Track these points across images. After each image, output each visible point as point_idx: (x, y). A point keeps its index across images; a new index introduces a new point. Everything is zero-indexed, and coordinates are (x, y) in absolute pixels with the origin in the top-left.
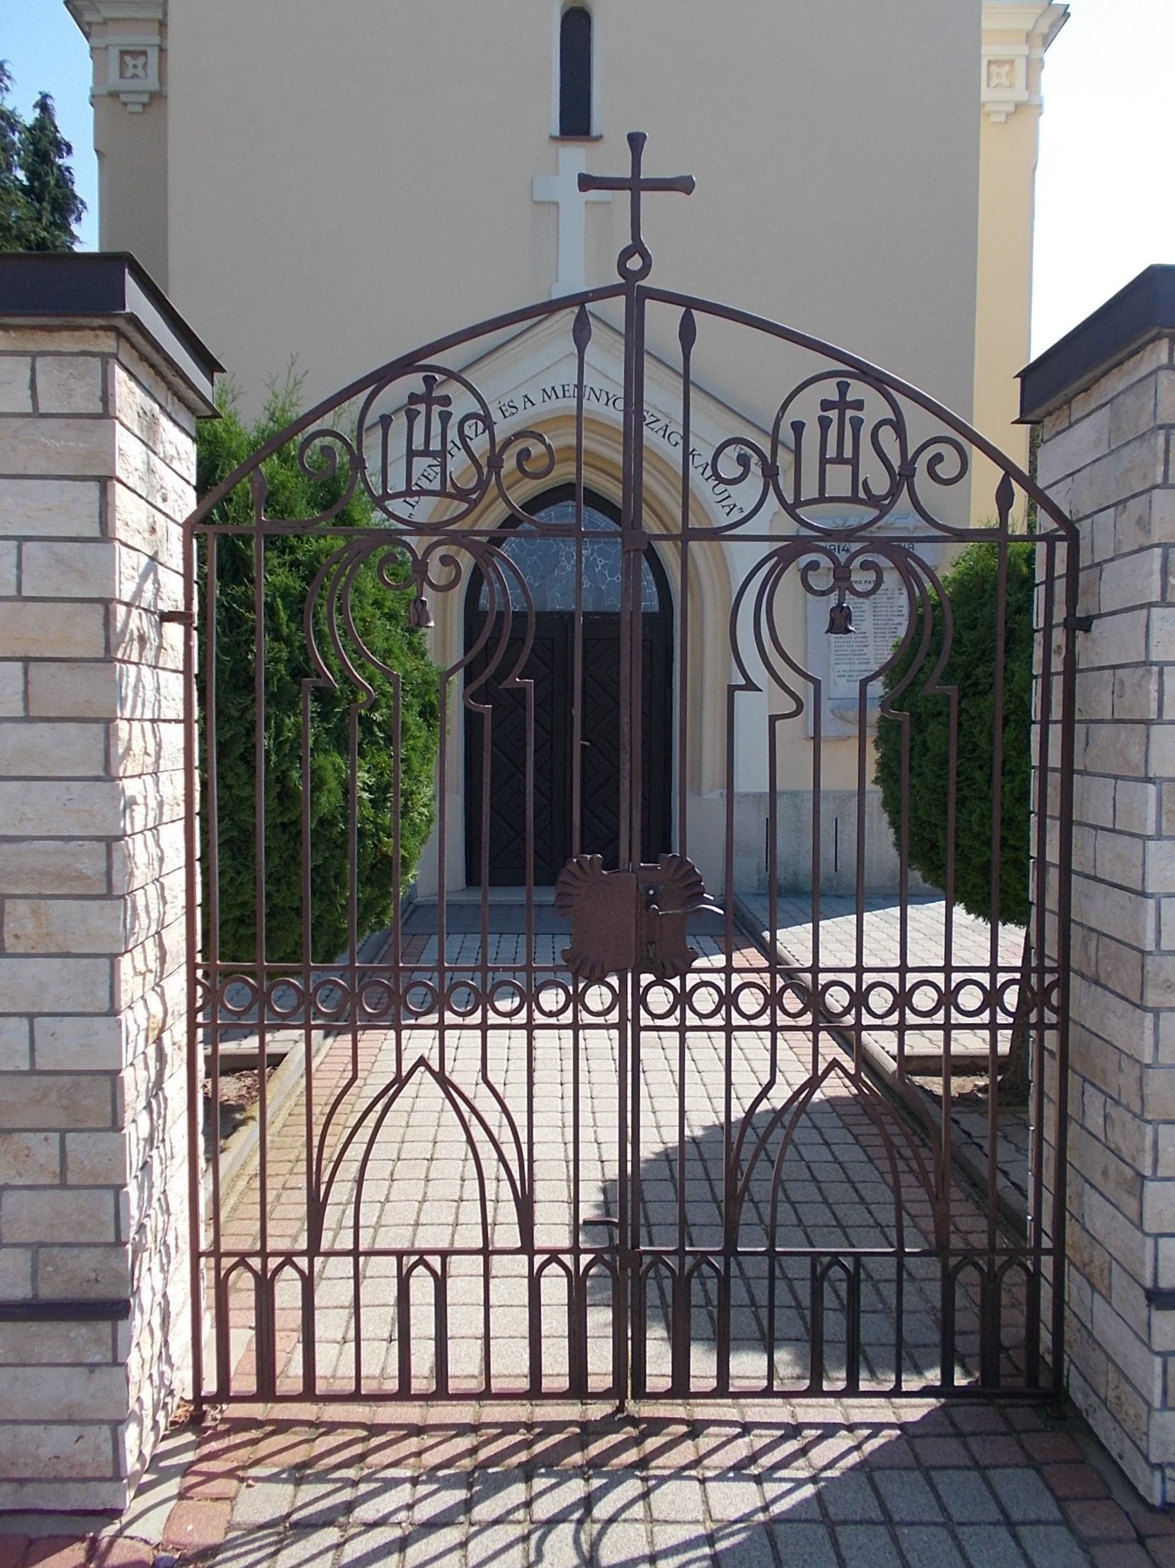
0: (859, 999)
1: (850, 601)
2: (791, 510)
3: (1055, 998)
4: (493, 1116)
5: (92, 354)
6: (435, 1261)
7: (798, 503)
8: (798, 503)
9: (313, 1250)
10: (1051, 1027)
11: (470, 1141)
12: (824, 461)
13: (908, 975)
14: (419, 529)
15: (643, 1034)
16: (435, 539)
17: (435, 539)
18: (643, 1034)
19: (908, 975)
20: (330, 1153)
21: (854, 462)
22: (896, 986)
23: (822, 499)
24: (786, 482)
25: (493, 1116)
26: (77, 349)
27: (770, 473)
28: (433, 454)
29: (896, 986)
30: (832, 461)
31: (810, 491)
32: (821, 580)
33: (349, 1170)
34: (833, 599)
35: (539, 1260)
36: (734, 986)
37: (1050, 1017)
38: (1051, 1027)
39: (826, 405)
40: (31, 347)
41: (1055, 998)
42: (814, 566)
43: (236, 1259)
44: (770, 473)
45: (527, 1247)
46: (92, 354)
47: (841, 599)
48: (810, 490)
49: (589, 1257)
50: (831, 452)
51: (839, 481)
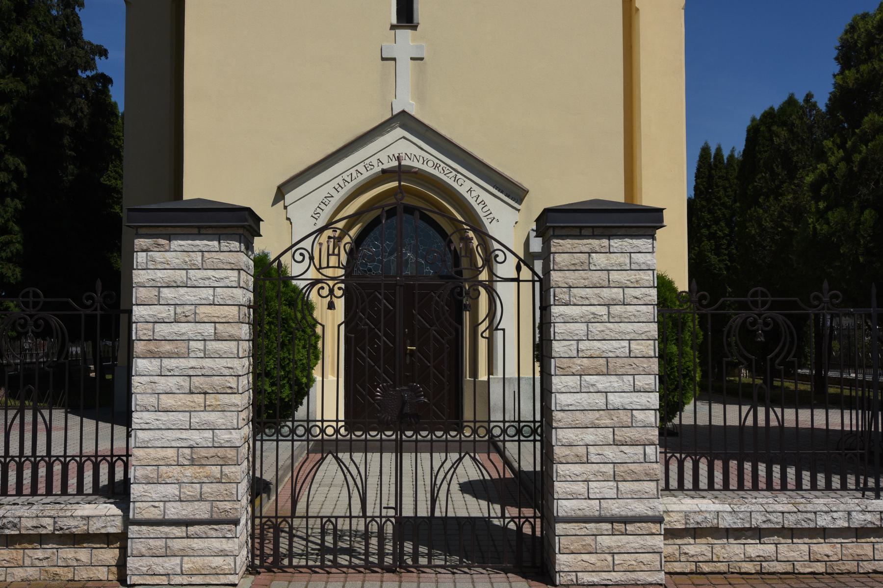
0: (504, 431)
1: (334, 299)
2: (318, 270)
3: (539, 430)
4: (354, 472)
5: (237, 234)
6: (333, 520)
7: (321, 268)
8: (321, 268)
9: (293, 515)
10: (538, 441)
11: (346, 478)
12: (329, 255)
13: (324, 423)
14: (332, 279)
15: (403, 443)
16: (336, 282)
17: (336, 282)
18: (403, 443)
19: (324, 423)
20: (438, 482)
21: (339, 255)
22: (473, 427)
23: (328, 267)
24: (316, 261)
25: (354, 472)
26: (232, 232)
27: (312, 258)
28: (336, 255)
29: (473, 427)
30: (331, 255)
31: (324, 264)
32: (325, 292)
33: (445, 486)
34: (329, 298)
35: (368, 520)
36: (310, 426)
37: (538, 438)
38: (538, 441)
39: (329, 238)
40: (219, 232)
41: (539, 430)
42: (322, 288)
43: (267, 519)
44: (312, 258)
45: (364, 516)
46: (237, 234)
47: (331, 298)
48: (324, 264)
49: (281, 520)
50: (331, 252)
51: (333, 261)
